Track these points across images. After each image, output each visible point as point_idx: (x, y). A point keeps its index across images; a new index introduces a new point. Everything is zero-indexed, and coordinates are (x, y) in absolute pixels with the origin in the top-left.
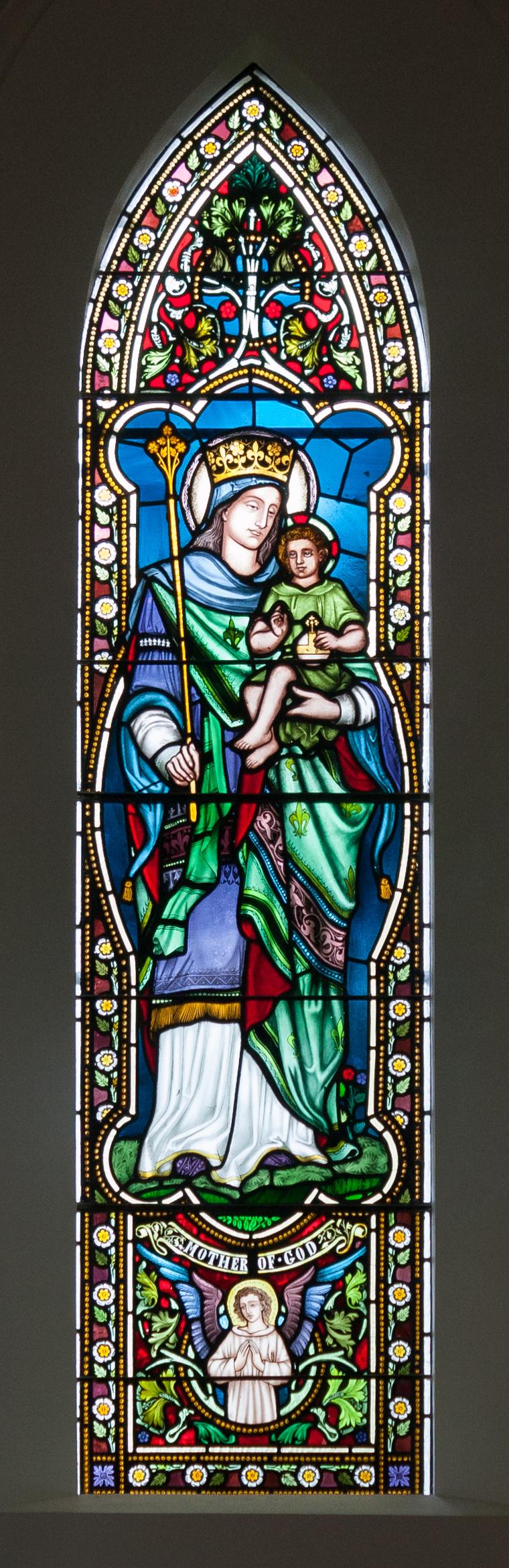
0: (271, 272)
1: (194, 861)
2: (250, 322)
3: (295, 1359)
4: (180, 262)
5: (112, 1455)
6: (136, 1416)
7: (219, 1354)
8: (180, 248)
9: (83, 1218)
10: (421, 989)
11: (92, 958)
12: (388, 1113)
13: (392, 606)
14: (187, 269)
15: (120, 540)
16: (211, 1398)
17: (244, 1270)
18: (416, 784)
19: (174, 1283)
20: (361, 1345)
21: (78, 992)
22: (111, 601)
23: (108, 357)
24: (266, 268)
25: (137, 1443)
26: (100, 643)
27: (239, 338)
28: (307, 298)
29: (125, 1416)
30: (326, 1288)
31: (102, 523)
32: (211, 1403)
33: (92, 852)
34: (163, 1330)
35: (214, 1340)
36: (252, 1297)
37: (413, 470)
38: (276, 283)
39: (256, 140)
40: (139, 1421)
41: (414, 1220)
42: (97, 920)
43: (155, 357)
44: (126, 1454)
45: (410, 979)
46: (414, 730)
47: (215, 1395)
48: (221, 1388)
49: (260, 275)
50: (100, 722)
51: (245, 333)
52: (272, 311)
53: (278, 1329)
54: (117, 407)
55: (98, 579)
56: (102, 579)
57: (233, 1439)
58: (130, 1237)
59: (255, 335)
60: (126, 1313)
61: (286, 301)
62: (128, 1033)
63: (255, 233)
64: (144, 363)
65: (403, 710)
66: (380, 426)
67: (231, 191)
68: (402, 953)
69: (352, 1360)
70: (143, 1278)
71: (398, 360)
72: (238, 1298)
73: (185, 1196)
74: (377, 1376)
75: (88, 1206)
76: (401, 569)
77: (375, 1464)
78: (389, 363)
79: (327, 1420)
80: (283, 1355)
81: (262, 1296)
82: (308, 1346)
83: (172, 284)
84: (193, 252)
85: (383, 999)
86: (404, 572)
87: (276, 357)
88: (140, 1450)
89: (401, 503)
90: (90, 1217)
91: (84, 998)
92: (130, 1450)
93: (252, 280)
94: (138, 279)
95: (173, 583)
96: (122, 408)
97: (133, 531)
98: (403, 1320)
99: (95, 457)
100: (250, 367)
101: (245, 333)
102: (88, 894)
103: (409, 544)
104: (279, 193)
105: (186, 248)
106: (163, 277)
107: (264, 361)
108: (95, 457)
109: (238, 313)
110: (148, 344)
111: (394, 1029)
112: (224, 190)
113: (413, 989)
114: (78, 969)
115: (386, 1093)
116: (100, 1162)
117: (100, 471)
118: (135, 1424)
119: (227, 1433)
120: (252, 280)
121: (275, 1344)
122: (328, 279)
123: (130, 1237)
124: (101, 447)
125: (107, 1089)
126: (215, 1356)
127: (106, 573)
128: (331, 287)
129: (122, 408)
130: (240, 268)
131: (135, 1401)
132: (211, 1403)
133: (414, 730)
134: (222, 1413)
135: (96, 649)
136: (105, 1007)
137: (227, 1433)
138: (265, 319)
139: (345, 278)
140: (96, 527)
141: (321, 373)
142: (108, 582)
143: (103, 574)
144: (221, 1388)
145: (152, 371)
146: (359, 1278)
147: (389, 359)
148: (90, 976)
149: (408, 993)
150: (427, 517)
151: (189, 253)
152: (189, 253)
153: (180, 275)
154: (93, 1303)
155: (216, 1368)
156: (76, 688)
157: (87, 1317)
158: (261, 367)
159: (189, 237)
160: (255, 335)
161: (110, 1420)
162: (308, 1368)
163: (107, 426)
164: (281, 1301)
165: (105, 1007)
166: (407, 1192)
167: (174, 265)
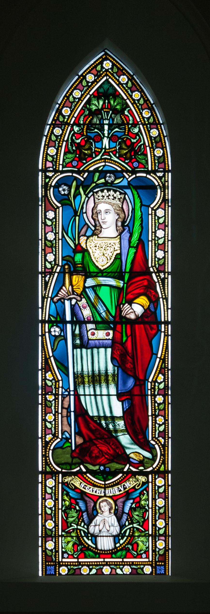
0: (113, 124)
1: (83, 83)
2: (106, 141)
3: (122, 527)
4: (79, 120)
5: (53, 562)
6: (62, 548)
7: (93, 524)
8: (79, 116)
9: (42, 476)
10: (168, 392)
11: (44, 379)
12: (157, 438)
13: (157, 251)
14: (82, 122)
15: (55, 519)
16: (90, 541)
17: (103, 495)
18: (166, 329)
19: (76, 499)
20: (146, 521)
21: (40, 392)
22: (52, 522)
23: (50, 422)
24: (111, 122)
25: (63, 557)
26: (48, 229)
27: (102, 149)
28: (126, 133)
29: (58, 548)
30: (131, 501)
31: (49, 492)
32: (89, 542)
33: (44, 461)
34: (73, 517)
35: (92, 518)
36: (105, 503)
37: (164, 200)
38: (115, 128)
39: (106, 75)
40: (64, 550)
41: (165, 476)
42: (47, 368)
43: (70, 156)
44: (59, 562)
45: (164, 388)
46: (165, 295)
47: (91, 540)
48: (94, 537)
49: (109, 125)
50: (49, 446)
51: (104, 147)
52: (112, 138)
53: (115, 514)
54: (53, 175)
55: (48, 555)
56: (49, 513)
57: (97, 556)
58: (60, 481)
59: (107, 147)
60: (59, 509)
61: (119, 135)
62: (58, 409)
63: (108, 108)
64: (65, 158)
65: (161, 284)
66: (153, 184)
67: (98, 95)
68: (161, 378)
69: (142, 526)
70: (65, 498)
71: (161, 257)
72: (99, 504)
73: (81, 469)
74: (152, 535)
75: (44, 473)
76: (161, 527)
77: (151, 565)
78: (158, 258)
79: (133, 549)
80: (116, 524)
81: (109, 504)
82: (125, 522)
83: (76, 129)
84: (84, 117)
85: (154, 396)
86: (162, 528)
87: (115, 155)
88: (64, 560)
89: (160, 213)
90: (45, 476)
91: (42, 395)
92: (60, 560)
93: (106, 127)
94: (63, 126)
95: (75, 239)
96: (56, 176)
97: (60, 241)
98: (162, 430)
99: (46, 193)
100: (105, 159)
101: (104, 147)
102: (44, 361)
103: (163, 393)
104: (116, 95)
105: (81, 115)
106: (72, 126)
107: (111, 157)
108: (46, 193)
109: (101, 139)
110: (67, 150)
111: (158, 552)
112: (96, 94)
113: (165, 391)
114: (40, 196)
115: (155, 430)
116: (49, 457)
117: (48, 198)
118: (62, 551)
119: (96, 553)
120: (106, 127)
121: (113, 519)
122: (135, 127)
123: (60, 481)
124: (48, 190)
125: (51, 494)
126: (91, 525)
127: (51, 553)
128: (136, 130)
129: (56, 176)
130: (102, 122)
131: (62, 542)
132: (89, 542)
133: (165, 295)
134: (94, 546)
135: (47, 433)
136: (50, 398)
137: (96, 553)
138: (111, 141)
139: (141, 126)
140: (46, 494)
141: (132, 161)
142: (51, 514)
143: (49, 511)
144: (94, 537)
145: (67, 161)
146: (145, 497)
147: (158, 257)
148: (45, 387)
149: (163, 393)
150: (170, 436)
151: (82, 117)
152: (82, 117)
153: (79, 125)
154: (46, 507)
155: (91, 529)
156: (39, 248)
157: (43, 426)
158: (110, 159)
159: (83, 111)
160: (107, 147)
161: (52, 421)
162: (125, 532)
163: (50, 184)
164: (116, 505)
165: (50, 398)
166: (163, 465)
167: (77, 122)
